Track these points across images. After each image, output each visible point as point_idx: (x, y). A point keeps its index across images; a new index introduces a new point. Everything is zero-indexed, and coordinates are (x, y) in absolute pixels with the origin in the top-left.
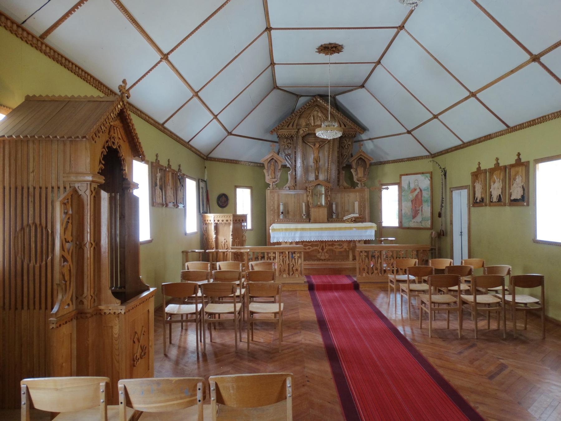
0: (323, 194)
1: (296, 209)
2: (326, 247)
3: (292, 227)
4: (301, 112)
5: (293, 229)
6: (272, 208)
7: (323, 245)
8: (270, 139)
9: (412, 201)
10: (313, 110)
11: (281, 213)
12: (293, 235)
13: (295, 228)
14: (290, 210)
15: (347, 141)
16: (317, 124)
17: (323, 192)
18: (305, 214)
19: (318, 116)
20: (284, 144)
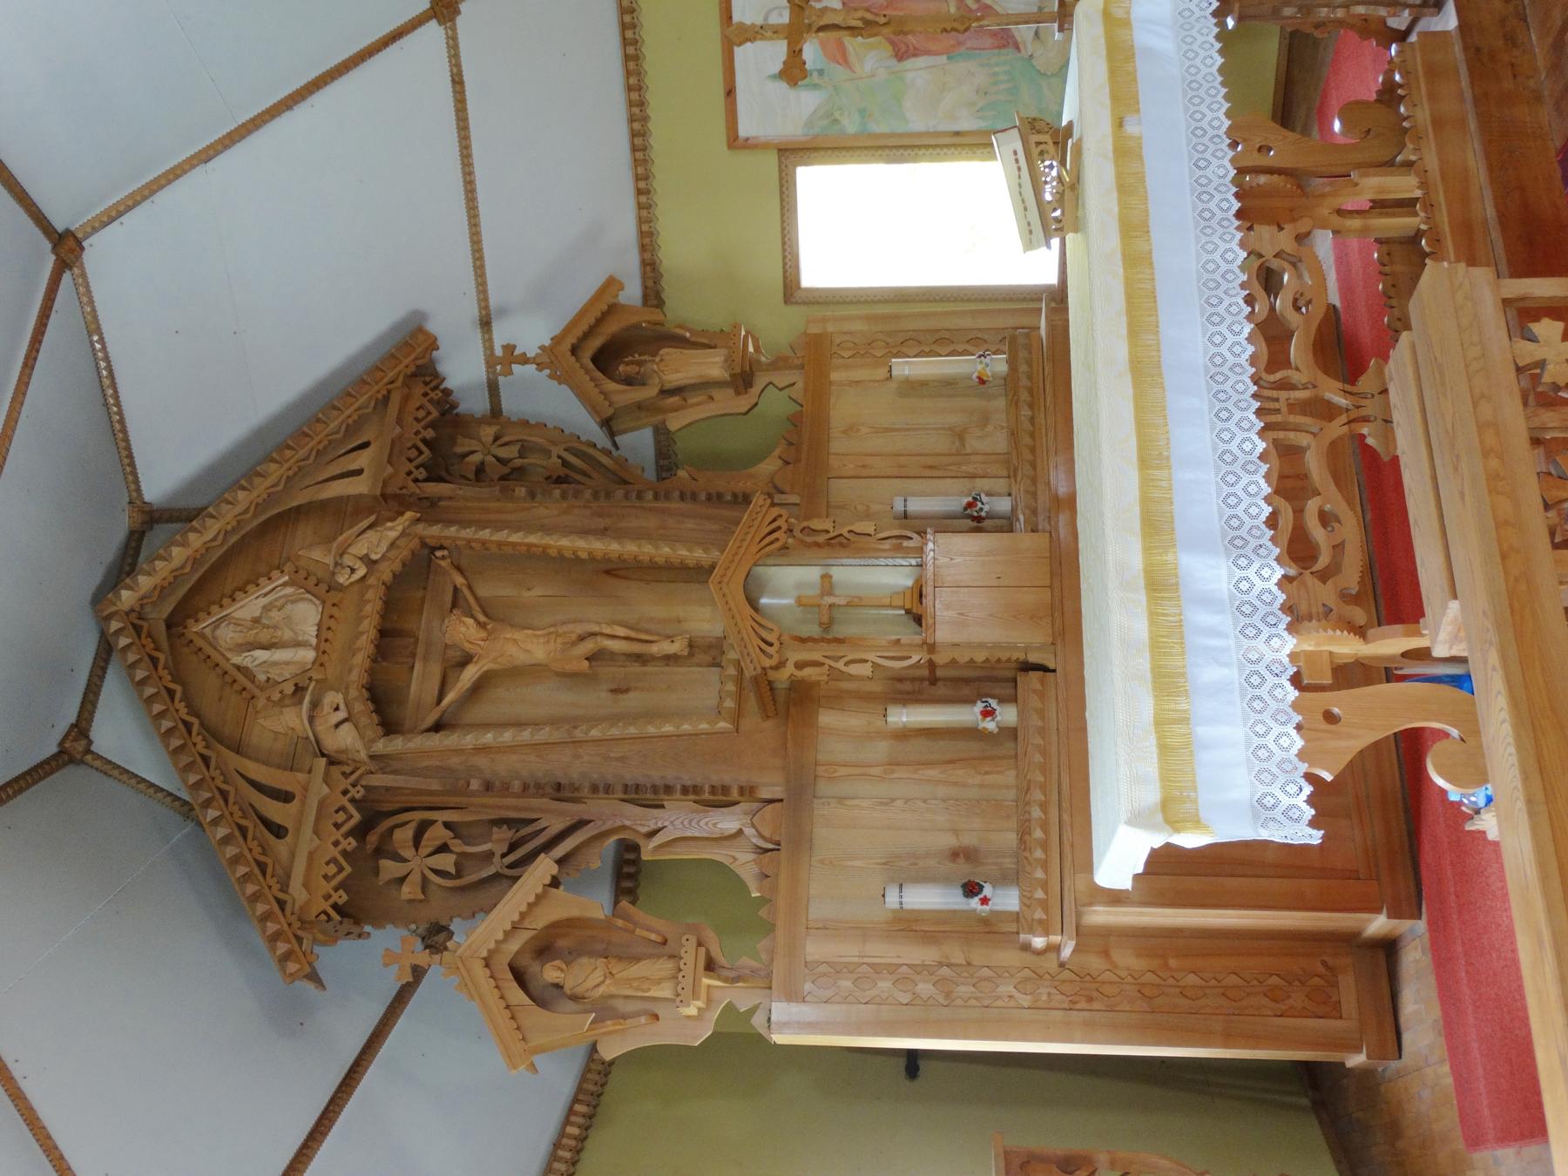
0: (826, 577)
1: (942, 791)
2: (1295, 377)
3: (1140, 627)
4: (188, 725)
5: (1153, 616)
6: (925, 988)
7: (1282, 405)
8: (376, 1011)
9: (901, 56)
10: (209, 650)
11: (974, 903)
12: (1223, 621)
13: (1142, 597)
14: (948, 841)
15: (474, 445)
16: (313, 631)
17: (811, 574)
18: (979, 706)
19: (256, 621)
20: (415, 878)
